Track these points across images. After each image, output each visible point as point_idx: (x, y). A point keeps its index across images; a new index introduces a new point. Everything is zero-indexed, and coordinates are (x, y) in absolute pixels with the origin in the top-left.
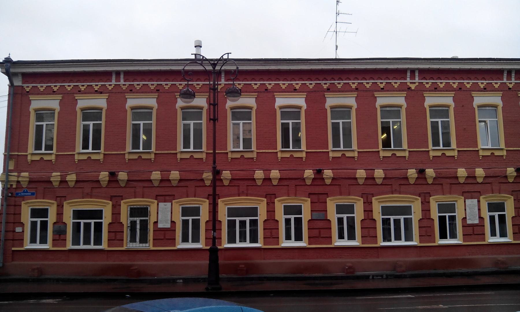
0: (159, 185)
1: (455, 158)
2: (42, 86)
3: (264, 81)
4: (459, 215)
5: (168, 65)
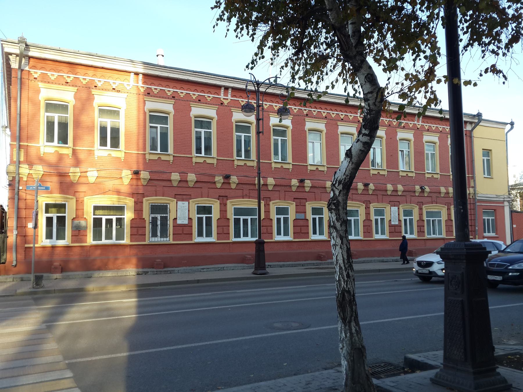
3: (177, 89)
4: (387, 218)
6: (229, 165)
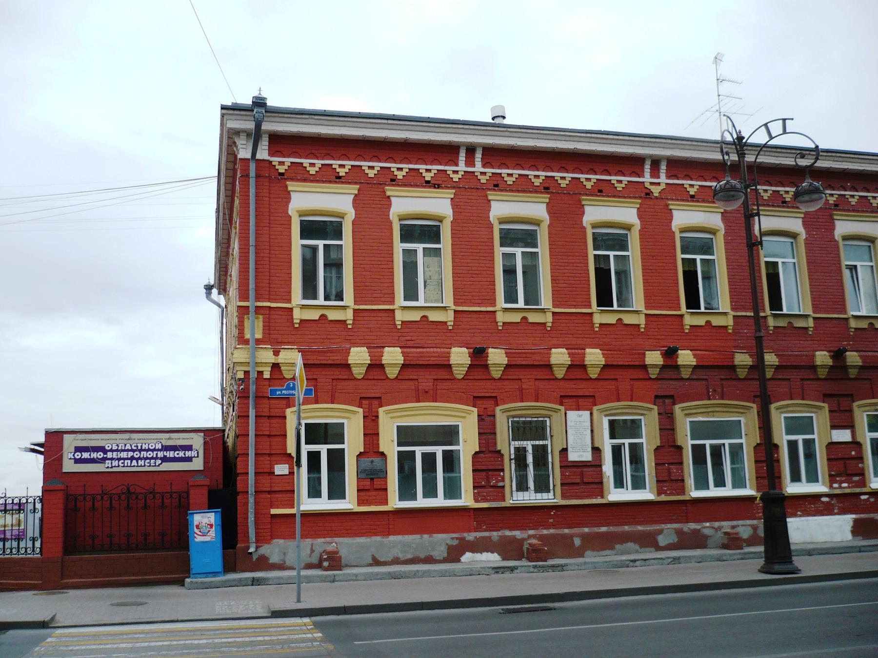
0: (692, 374)
1: (347, 325)
2: (313, 164)
3: (301, 157)
5: (572, 140)
6: (672, 327)
